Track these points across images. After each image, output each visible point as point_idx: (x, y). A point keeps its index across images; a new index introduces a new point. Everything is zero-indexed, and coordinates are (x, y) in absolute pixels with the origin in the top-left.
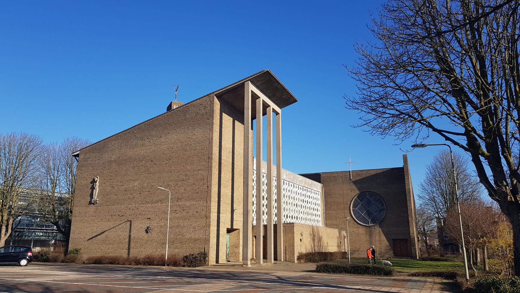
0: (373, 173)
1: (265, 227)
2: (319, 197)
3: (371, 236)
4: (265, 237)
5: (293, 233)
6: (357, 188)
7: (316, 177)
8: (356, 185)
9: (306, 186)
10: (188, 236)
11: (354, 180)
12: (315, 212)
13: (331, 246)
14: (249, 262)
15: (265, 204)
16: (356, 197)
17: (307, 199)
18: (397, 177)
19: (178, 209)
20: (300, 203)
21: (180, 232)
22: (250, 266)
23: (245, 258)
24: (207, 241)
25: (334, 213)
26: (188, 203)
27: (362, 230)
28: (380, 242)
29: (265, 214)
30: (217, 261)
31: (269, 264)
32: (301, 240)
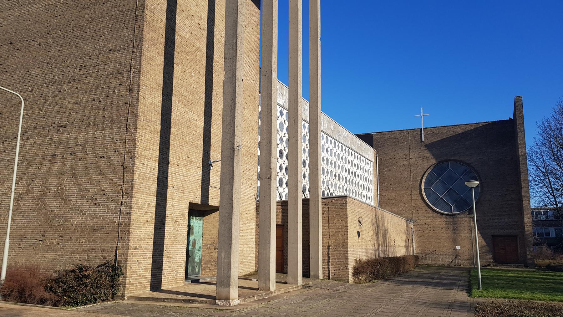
0: (460, 131)
1: (283, 205)
2: (371, 170)
3: (455, 229)
4: (282, 228)
5: (345, 217)
6: (433, 155)
7: (367, 138)
8: (430, 151)
9: (354, 148)
10: (78, 219)
11: (427, 143)
12: (365, 192)
13: (399, 246)
14: (234, 292)
15: (284, 167)
16: (430, 170)
17: (354, 169)
18: (505, 133)
19: (60, 150)
20: (344, 175)
21: (60, 209)
22: (235, 301)
23: (224, 281)
24: (123, 230)
25: (393, 194)
26: (81, 137)
27: (440, 222)
28: (470, 242)
29: (284, 185)
30: (156, 285)
31: (291, 288)
32: (358, 233)
